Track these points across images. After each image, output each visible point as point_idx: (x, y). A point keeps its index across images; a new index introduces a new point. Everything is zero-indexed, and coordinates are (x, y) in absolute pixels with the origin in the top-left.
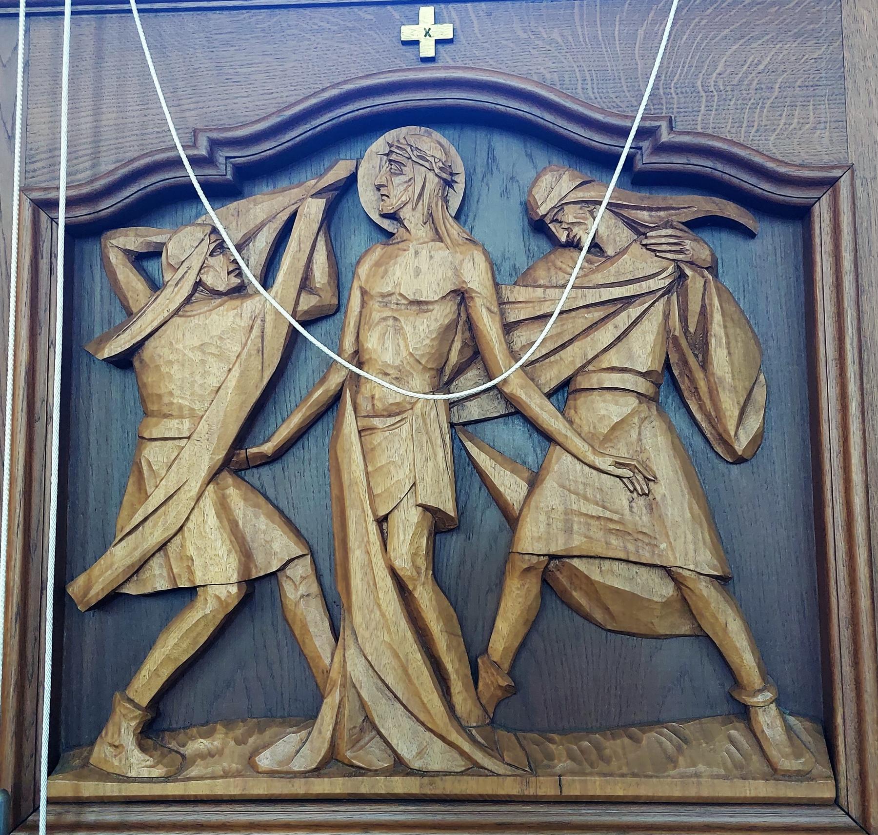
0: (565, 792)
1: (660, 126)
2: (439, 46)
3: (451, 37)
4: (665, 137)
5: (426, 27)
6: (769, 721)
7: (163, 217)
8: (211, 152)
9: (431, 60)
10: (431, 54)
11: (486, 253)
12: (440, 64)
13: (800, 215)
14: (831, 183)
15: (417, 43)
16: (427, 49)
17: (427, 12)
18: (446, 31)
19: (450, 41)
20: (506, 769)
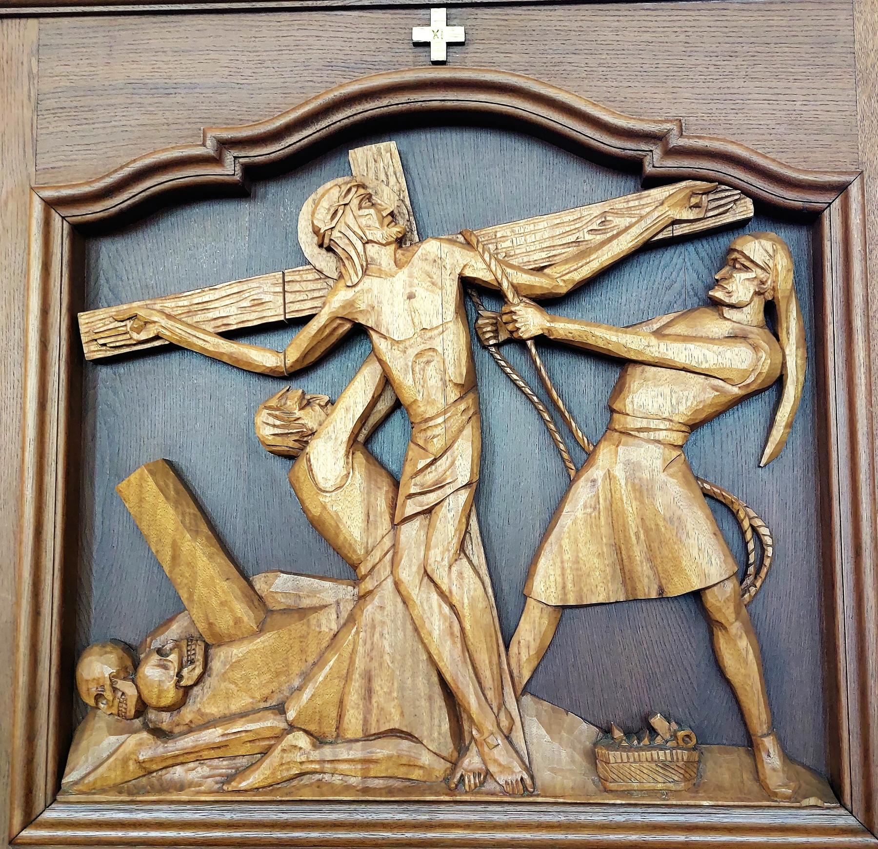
0: (439, 243)
1: (669, 131)
2: (452, 50)
3: (463, 40)
4: (675, 141)
5: (439, 30)
6: (772, 758)
7: (168, 216)
8: (220, 154)
9: (443, 63)
10: (442, 57)
11: (307, 732)
12: (451, 65)
13: (808, 220)
14: (842, 189)
15: (427, 44)
16: (438, 52)
17: (438, 15)
18: (457, 34)
19: (461, 44)
20: (473, 600)
